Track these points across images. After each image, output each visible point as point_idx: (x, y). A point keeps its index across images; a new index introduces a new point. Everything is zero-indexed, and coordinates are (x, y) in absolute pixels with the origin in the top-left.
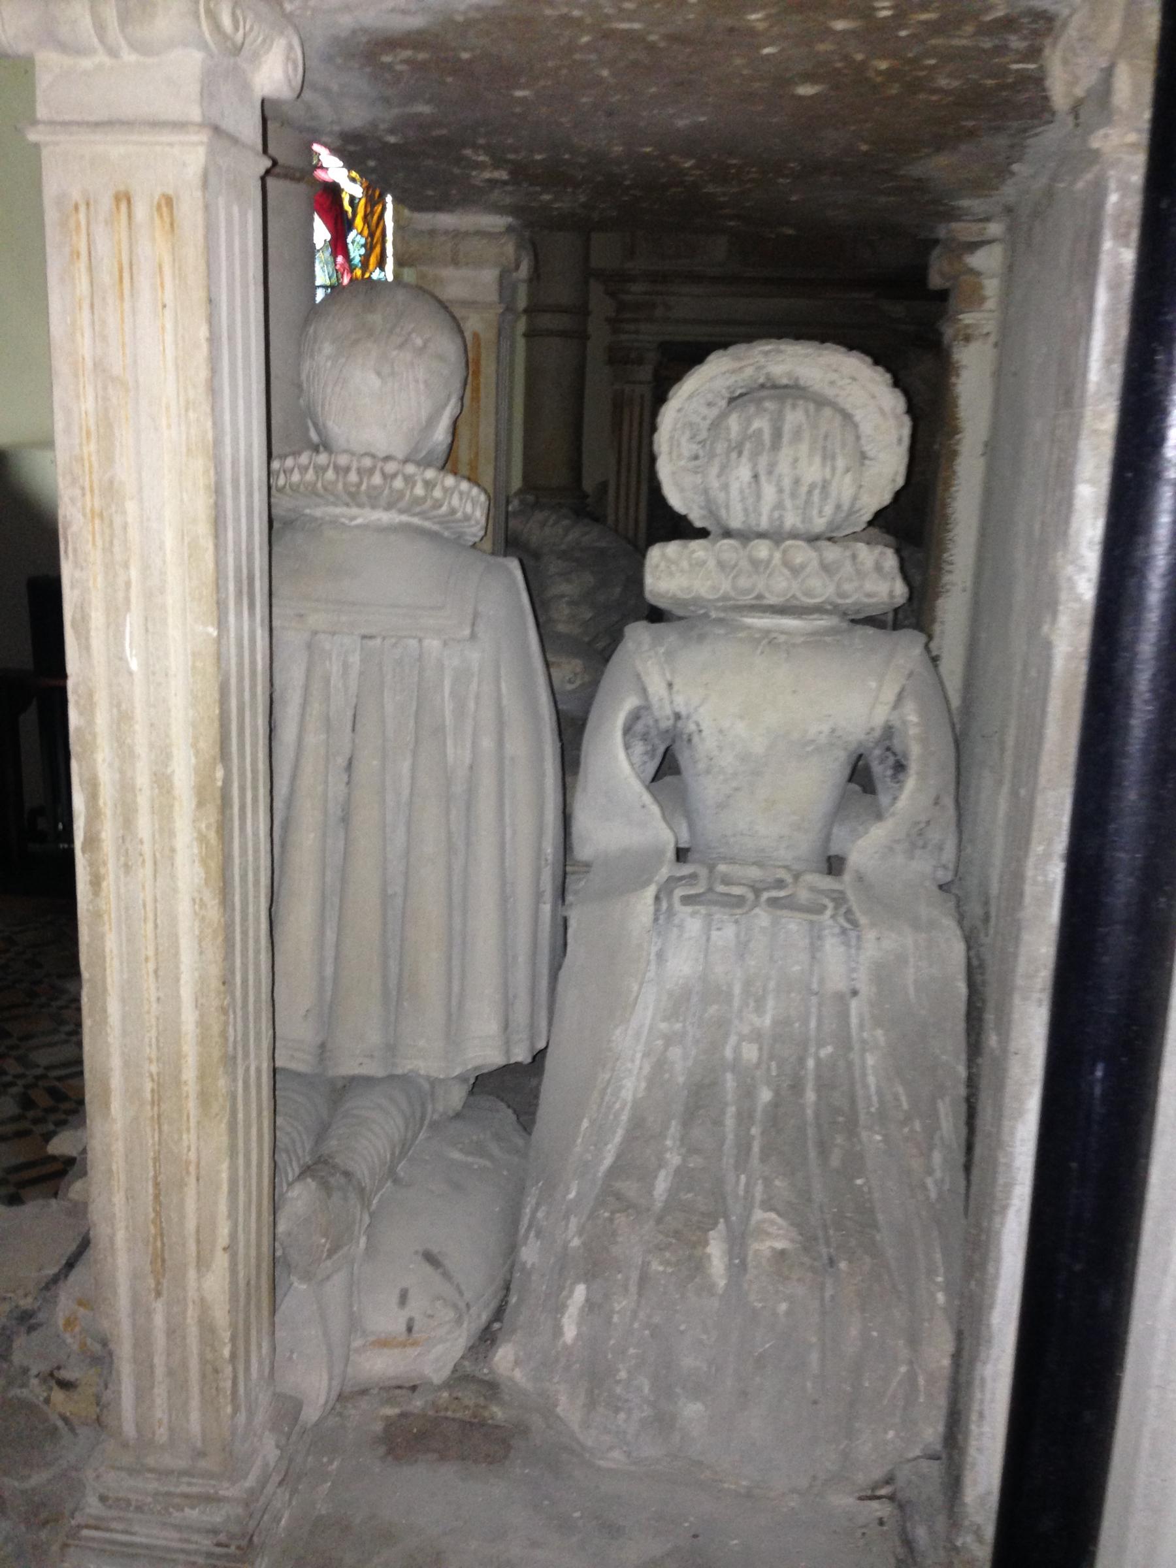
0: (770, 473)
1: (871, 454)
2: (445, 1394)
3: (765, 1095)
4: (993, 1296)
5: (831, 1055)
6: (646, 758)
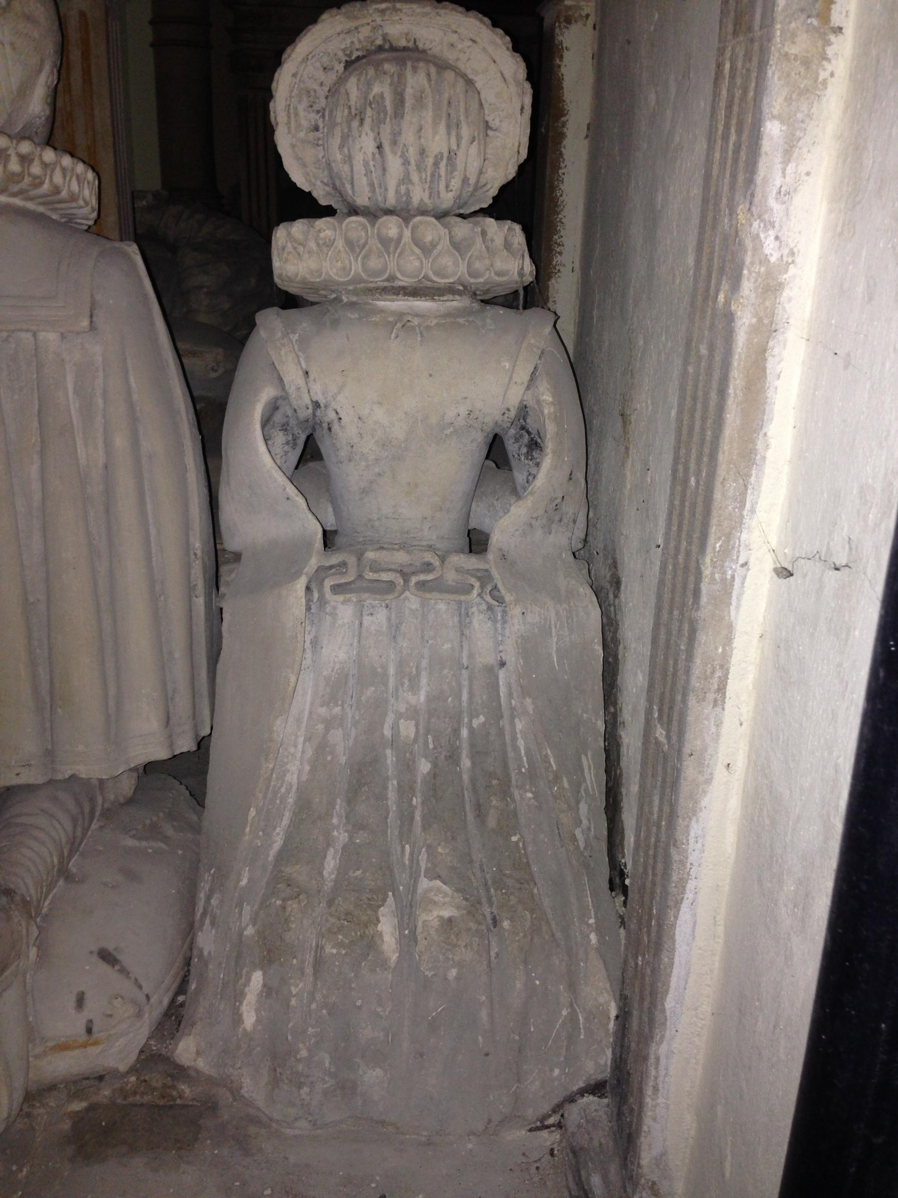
0: (394, 143)
1: (494, 124)
2: (133, 1079)
3: (424, 767)
4: (667, 984)
5: (484, 724)
6: (286, 448)
